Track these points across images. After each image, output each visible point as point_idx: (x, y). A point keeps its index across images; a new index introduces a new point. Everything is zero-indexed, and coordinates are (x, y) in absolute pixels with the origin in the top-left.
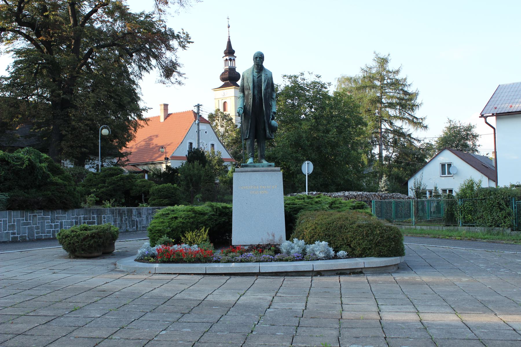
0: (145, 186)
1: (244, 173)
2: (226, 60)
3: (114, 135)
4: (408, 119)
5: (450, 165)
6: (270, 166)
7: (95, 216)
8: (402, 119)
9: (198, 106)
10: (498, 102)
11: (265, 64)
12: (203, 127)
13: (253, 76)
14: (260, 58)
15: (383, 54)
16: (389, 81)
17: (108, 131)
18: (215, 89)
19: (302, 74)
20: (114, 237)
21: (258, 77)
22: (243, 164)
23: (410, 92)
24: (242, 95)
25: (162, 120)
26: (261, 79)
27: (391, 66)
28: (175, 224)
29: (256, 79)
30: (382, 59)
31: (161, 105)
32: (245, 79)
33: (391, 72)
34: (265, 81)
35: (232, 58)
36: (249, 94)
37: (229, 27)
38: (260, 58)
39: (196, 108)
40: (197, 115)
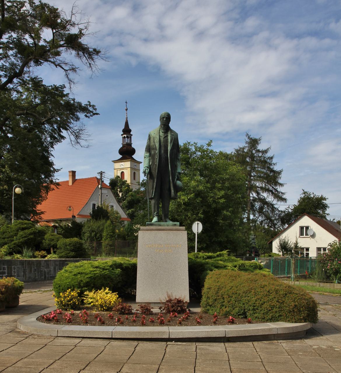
0: (53, 240)
1: (149, 231)
2: (124, 137)
3: (26, 193)
4: (271, 191)
5: (307, 228)
6: (175, 225)
7: (6, 267)
8: (268, 190)
9: (101, 173)
11: (172, 125)
12: (105, 191)
13: (160, 136)
14: (166, 118)
15: (254, 136)
17: (21, 190)
18: (115, 162)
20: (18, 290)
22: (149, 223)
23: (275, 169)
24: (148, 154)
25: (70, 184)
26: (167, 140)
27: (261, 147)
29: (162, 139)
31: (69, 172)
32: (152, 139)
35: (129, 136)
37: (127, 110)
38: (166, 118)
39: (99, 174)
40: (100, 181)
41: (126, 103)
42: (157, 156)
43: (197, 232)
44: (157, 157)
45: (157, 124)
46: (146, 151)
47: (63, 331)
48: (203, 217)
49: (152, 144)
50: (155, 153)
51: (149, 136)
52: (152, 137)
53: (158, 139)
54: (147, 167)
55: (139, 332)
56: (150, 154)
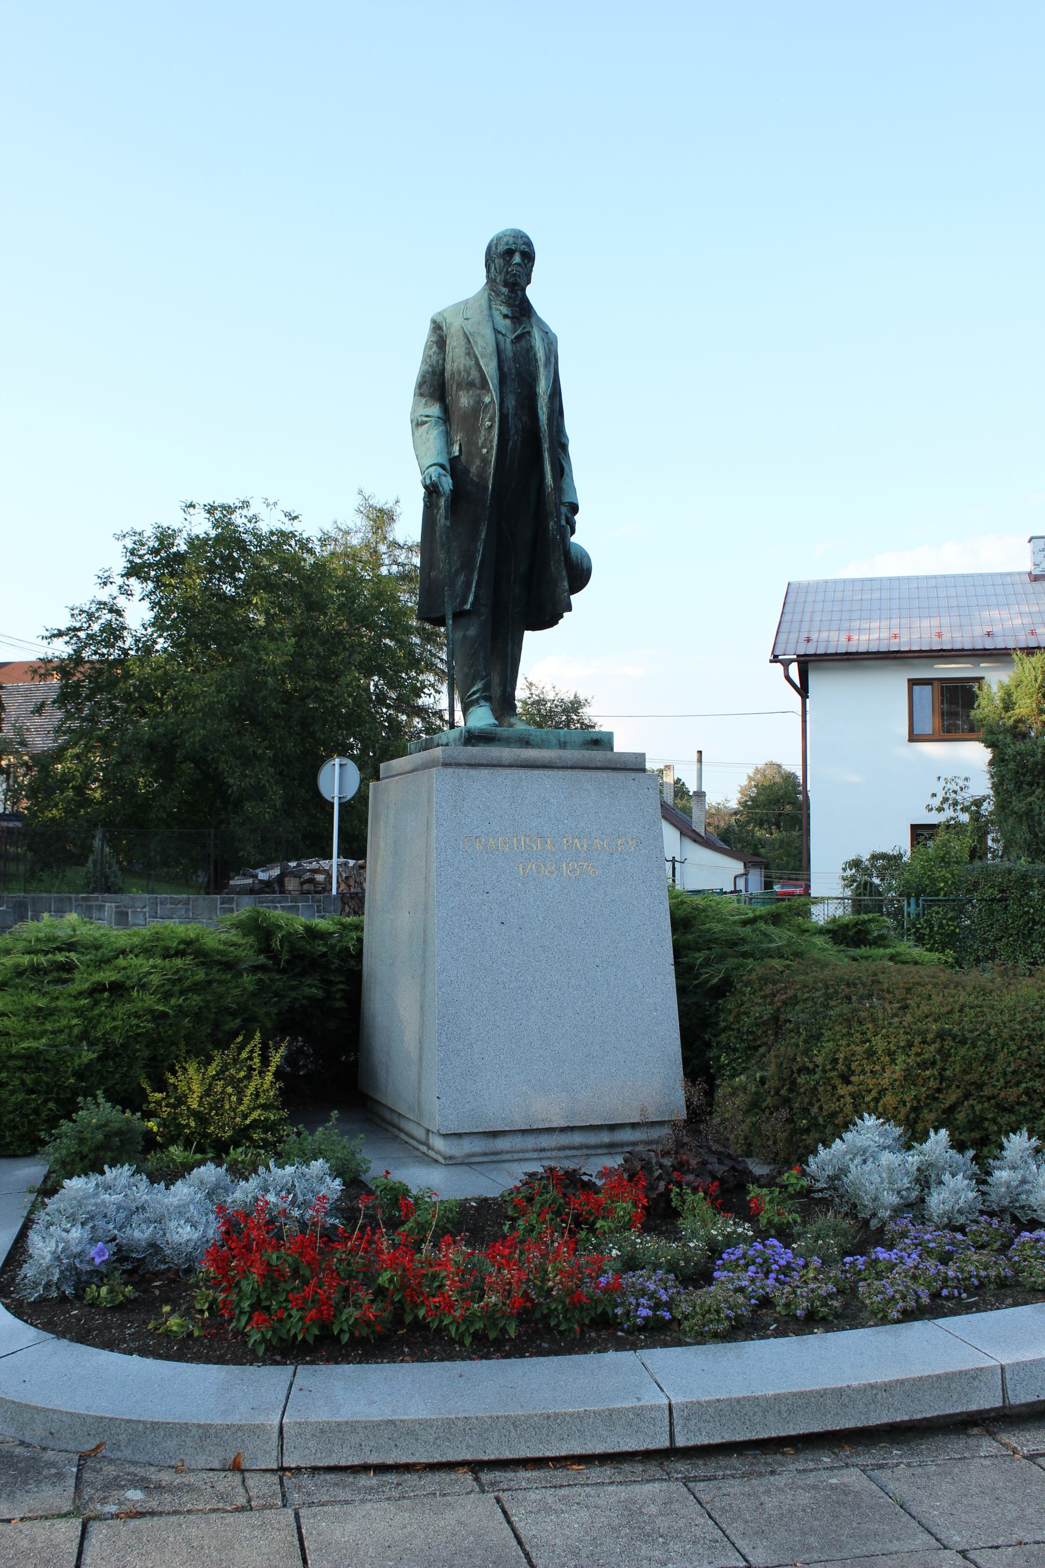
1: (485, 772)
10: (805, 626)
13: (496, 331)
16: (395, 569)
19: (246, 504)
21: (518, 338)
24: (435, 410)
28: (117, 1019)
30: (381, 511)
33: (401, 547)
36: (478, 408)
42: (492, 419)
43: (340, 798)
45: (472, 280)
46: (420, 385)
47: (324, 1431)
50: (479, 402)
54: (442, 466)
55: (839, 1392)
56: (446, 410)
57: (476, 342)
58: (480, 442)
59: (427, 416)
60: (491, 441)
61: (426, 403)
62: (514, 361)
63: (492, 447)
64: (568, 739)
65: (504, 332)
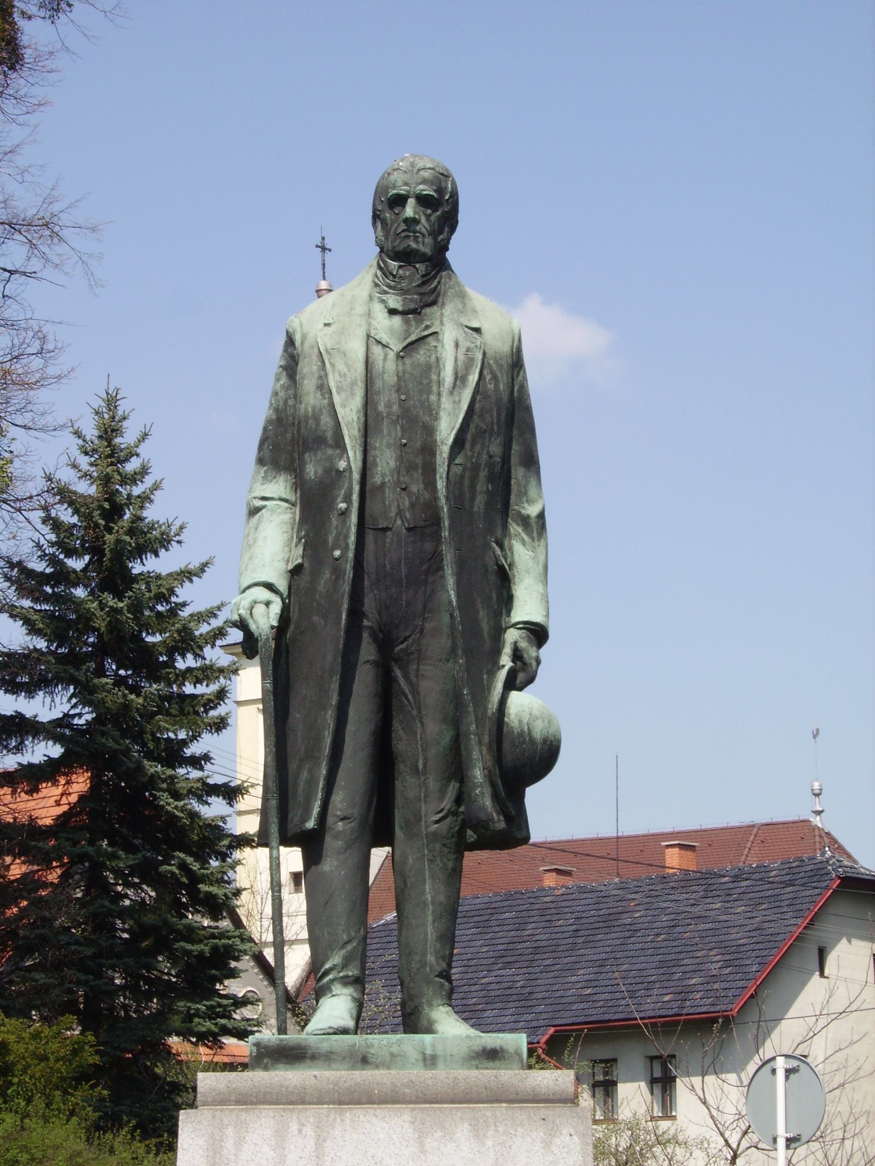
6: (492, 1055)
29: (388, 366)
32: (308, 368)
34: (460, 379)
41: (324, 249)
42: (348, 499)
44: (347, 502)
46: (261, 461)
48: (229, 964)
49: (311, 399)
51: (290, 341)
52: (303, 347)
53: (360, 367)
57: (333, 365)
58: (331, 539)
59: (264, 499)
60: (347, 537)
61: (265, 478)
62: (398, 391)
63: (347, 545)
64: (439, 1051)
65: (385, 339)
